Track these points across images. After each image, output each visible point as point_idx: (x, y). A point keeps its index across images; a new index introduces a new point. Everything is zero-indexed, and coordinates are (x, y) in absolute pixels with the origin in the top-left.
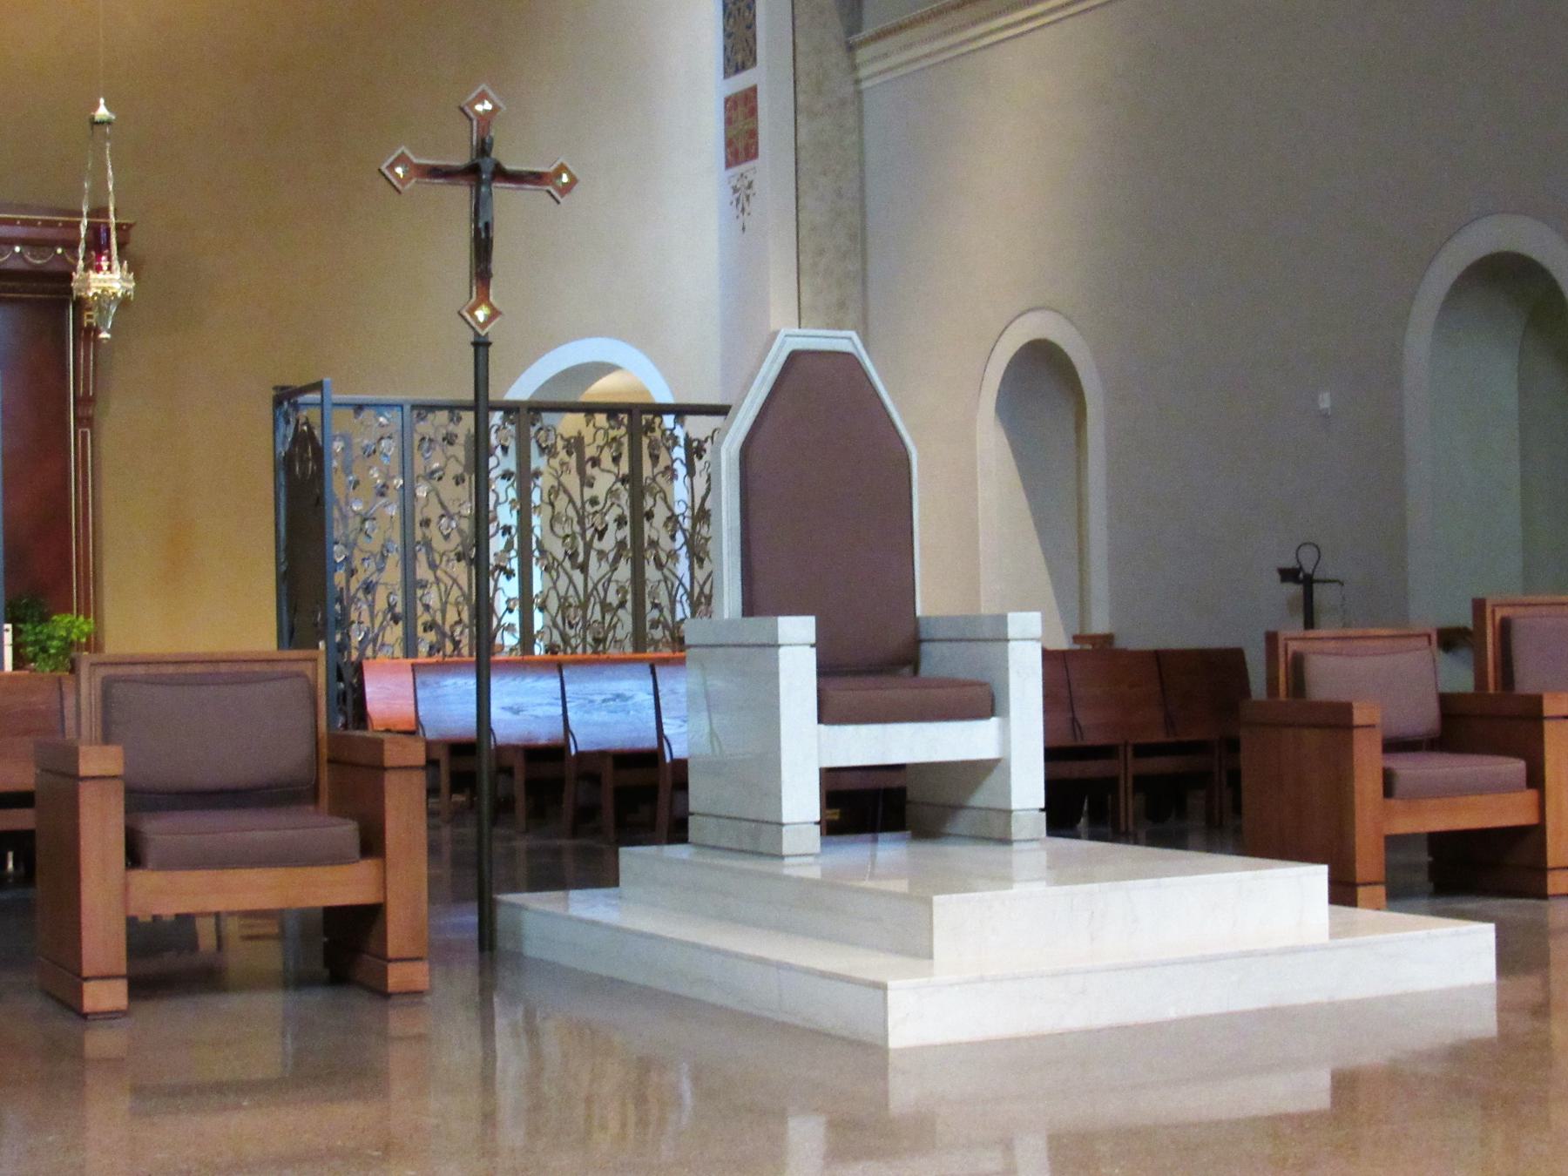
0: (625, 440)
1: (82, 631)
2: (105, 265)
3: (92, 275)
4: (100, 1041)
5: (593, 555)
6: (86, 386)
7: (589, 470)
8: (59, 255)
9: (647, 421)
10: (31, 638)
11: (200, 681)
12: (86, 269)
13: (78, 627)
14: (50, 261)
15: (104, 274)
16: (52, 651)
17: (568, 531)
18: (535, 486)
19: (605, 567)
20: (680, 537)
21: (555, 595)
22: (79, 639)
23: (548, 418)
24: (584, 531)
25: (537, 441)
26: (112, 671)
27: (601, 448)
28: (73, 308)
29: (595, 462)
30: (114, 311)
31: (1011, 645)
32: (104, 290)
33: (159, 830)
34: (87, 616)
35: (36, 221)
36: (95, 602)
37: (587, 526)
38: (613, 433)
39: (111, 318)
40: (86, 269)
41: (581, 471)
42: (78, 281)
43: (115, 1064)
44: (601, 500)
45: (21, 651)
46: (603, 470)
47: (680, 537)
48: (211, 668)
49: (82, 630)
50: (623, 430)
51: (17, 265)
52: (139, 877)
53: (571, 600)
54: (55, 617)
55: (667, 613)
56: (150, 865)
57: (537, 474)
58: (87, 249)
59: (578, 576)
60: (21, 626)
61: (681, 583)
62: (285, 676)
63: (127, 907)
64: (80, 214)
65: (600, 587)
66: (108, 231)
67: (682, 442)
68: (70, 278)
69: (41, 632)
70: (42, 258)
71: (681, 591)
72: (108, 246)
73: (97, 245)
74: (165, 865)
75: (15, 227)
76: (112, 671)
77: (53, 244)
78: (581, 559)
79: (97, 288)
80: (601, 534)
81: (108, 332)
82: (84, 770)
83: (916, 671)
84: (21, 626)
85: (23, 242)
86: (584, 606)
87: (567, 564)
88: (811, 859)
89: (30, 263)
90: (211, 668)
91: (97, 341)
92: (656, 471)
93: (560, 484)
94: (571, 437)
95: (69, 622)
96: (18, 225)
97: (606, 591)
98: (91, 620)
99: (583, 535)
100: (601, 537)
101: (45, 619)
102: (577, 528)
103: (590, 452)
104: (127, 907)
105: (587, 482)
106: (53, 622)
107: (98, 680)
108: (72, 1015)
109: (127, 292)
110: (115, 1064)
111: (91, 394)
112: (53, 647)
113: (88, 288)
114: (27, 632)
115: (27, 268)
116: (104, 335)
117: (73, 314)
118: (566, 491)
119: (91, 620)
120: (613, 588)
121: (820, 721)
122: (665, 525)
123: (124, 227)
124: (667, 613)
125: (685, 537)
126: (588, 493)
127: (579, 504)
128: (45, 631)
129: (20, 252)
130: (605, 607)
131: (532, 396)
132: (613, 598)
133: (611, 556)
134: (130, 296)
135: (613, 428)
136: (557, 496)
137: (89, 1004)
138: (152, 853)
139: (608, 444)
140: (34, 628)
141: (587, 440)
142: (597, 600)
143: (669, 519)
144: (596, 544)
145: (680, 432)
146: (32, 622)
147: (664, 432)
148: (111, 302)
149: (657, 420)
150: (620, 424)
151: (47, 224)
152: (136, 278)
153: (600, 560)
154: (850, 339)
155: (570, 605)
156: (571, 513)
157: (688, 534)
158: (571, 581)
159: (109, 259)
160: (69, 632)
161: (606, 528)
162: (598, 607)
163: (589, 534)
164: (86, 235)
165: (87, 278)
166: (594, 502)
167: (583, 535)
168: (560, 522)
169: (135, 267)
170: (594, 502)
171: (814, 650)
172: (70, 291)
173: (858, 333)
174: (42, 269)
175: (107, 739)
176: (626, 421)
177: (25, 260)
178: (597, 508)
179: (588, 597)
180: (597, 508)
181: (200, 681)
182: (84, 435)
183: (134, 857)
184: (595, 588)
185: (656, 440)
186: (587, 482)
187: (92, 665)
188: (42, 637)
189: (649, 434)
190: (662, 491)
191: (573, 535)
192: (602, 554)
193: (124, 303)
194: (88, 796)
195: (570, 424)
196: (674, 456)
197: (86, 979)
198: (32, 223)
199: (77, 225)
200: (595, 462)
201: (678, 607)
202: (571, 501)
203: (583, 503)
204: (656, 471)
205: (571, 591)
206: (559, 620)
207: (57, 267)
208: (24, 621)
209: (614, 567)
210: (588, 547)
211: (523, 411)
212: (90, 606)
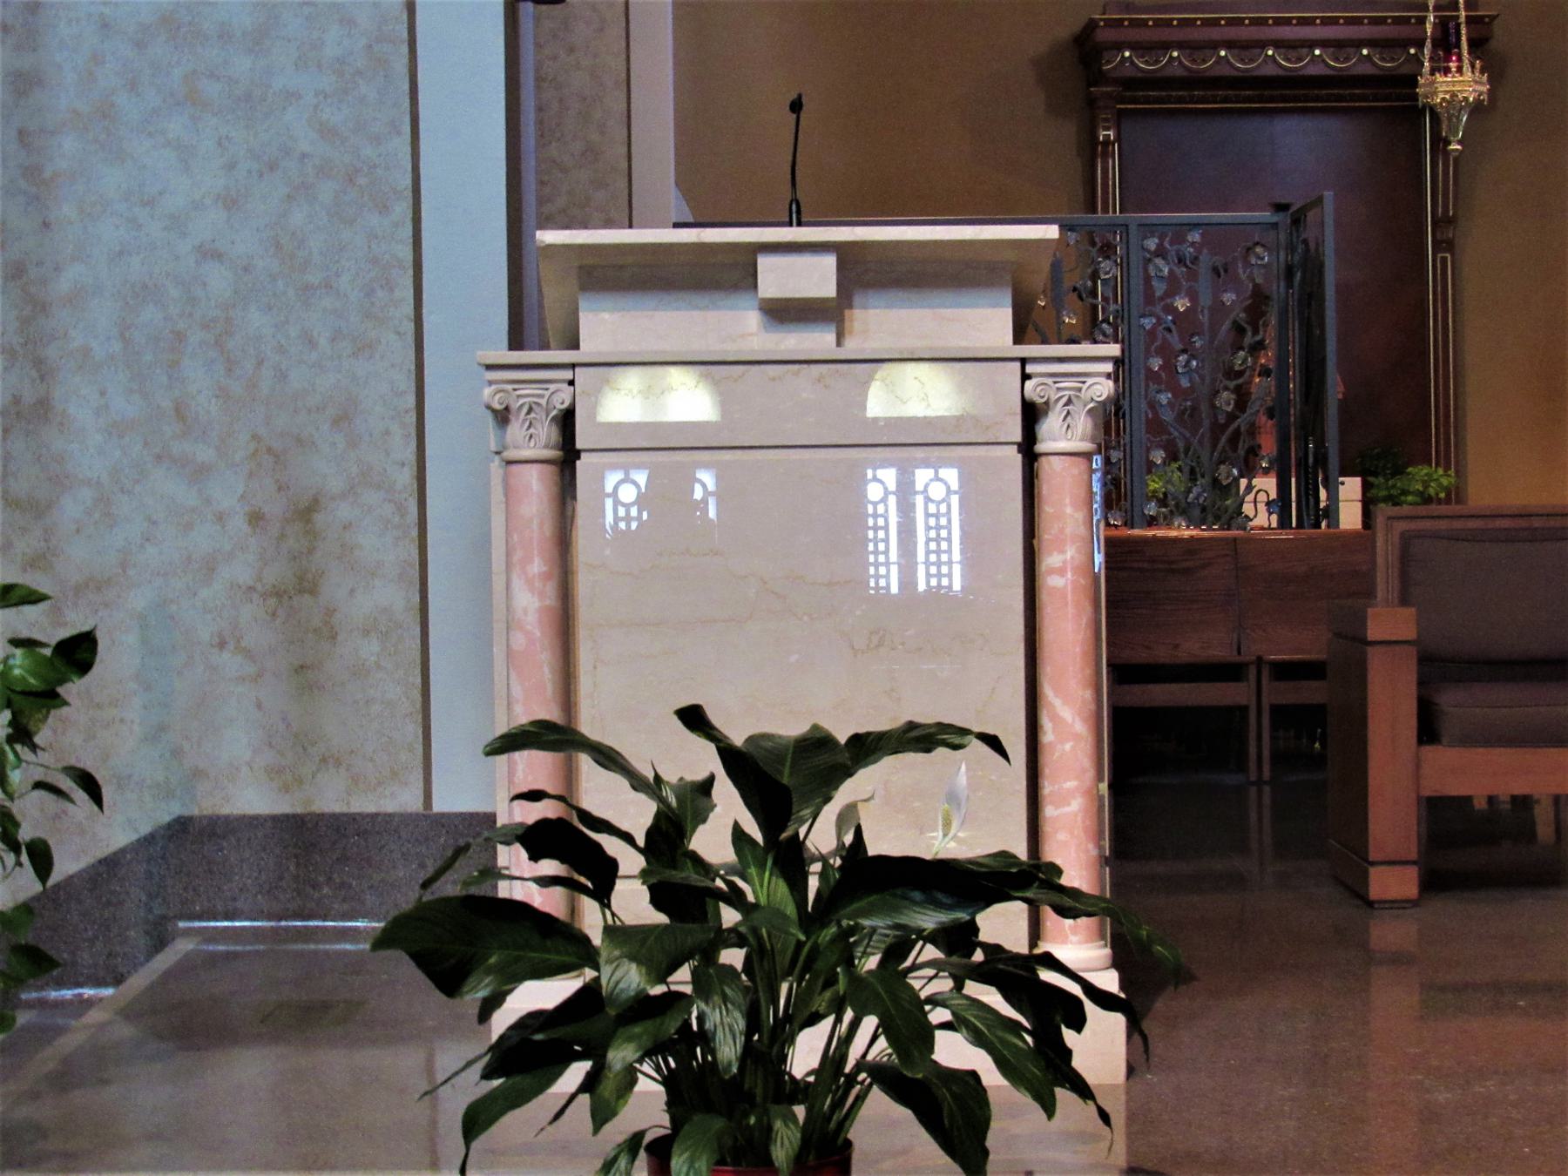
1: (1440, 485)
2: (1453, 65)
3: (1439, 78)
4: (1389, 933)
8: (1318, 56)
10: (1383, 493)
11: (1509, 537)
12: (1432, 72)
13: (1436, 480)
14: (1258, 67)
15: (1454, 77)
22: (1437, 494)
26: (1413, 525)
30: (1465, 119)
32: (1454, 95)
33: (1451, 700)
34: (1447, 468)
35: (1386, 18)
39: (1461, 128)
40: (1432, 72)
42: (1424, 85)
43: (1398, 960)
48: (1523, 523)
49: (1441, 483)
51: (1270, 70)
52: (1429, 752)
54: (1410, 469)
56: (1445, 740)
58: (1435, 45)
60: (1371, 479)
64: (1427, 10)
66: (1458, 25)
68: (1415, 84)
69: (1394, 486)
70: (1393, 60)
72: (1458, 45)
73: (1445, 43)
74: (1468, 740)
75: (1361, 28)
76: (1413, 525)
77: (1404, 44)
79: (1446, 92)
81: (1459, 142)
82: (1372, 634)
84: (1371, 479)
85: (1323, 44)
90: (1523, 523)
91: (1446, 153)
95: (1426, 475)
96: (1389, 24)
98: (1452, 472)
101: (1399, 471)
106: (1409, 474)
108: (1360, 902)
109: (1479, 96)
110: (1398, 960)
111: (1451, 214)
113: (1435, 93)
114: (1378, 486)
116: (1455, 146)
117: (1430, 122)
119: (1452, 472)
123: (1487, 20)
128: (1399, 485)
129: (1368, 55)
134: (1484, 100)
137: (1375, 892)
140: (1387, 480)
146: (1385, 475)
148: (1461, 108)
151: (1398, 21)
152: (1490, 81)
159: (1460, 59)
160: (1426, 485)
164: (1432, 33)
165: (1434, 82)
169: (1495, 69)
172: (1415, 97)
174: (1394, 73)
175: (1404, 601)
177: (1374, 64)
181: (1535, 536)
182: (1444, 260)
183: (1428, 731)
187: (1389, 518)
188: (1394, 492)
193: (1477, 109)
194: (1377, 664)
197: (1373, 864)
198: (1333, 21)
199: (1422, 21)
207: (1405, 70)
208: (1375, 474)
212: (1451, 456)
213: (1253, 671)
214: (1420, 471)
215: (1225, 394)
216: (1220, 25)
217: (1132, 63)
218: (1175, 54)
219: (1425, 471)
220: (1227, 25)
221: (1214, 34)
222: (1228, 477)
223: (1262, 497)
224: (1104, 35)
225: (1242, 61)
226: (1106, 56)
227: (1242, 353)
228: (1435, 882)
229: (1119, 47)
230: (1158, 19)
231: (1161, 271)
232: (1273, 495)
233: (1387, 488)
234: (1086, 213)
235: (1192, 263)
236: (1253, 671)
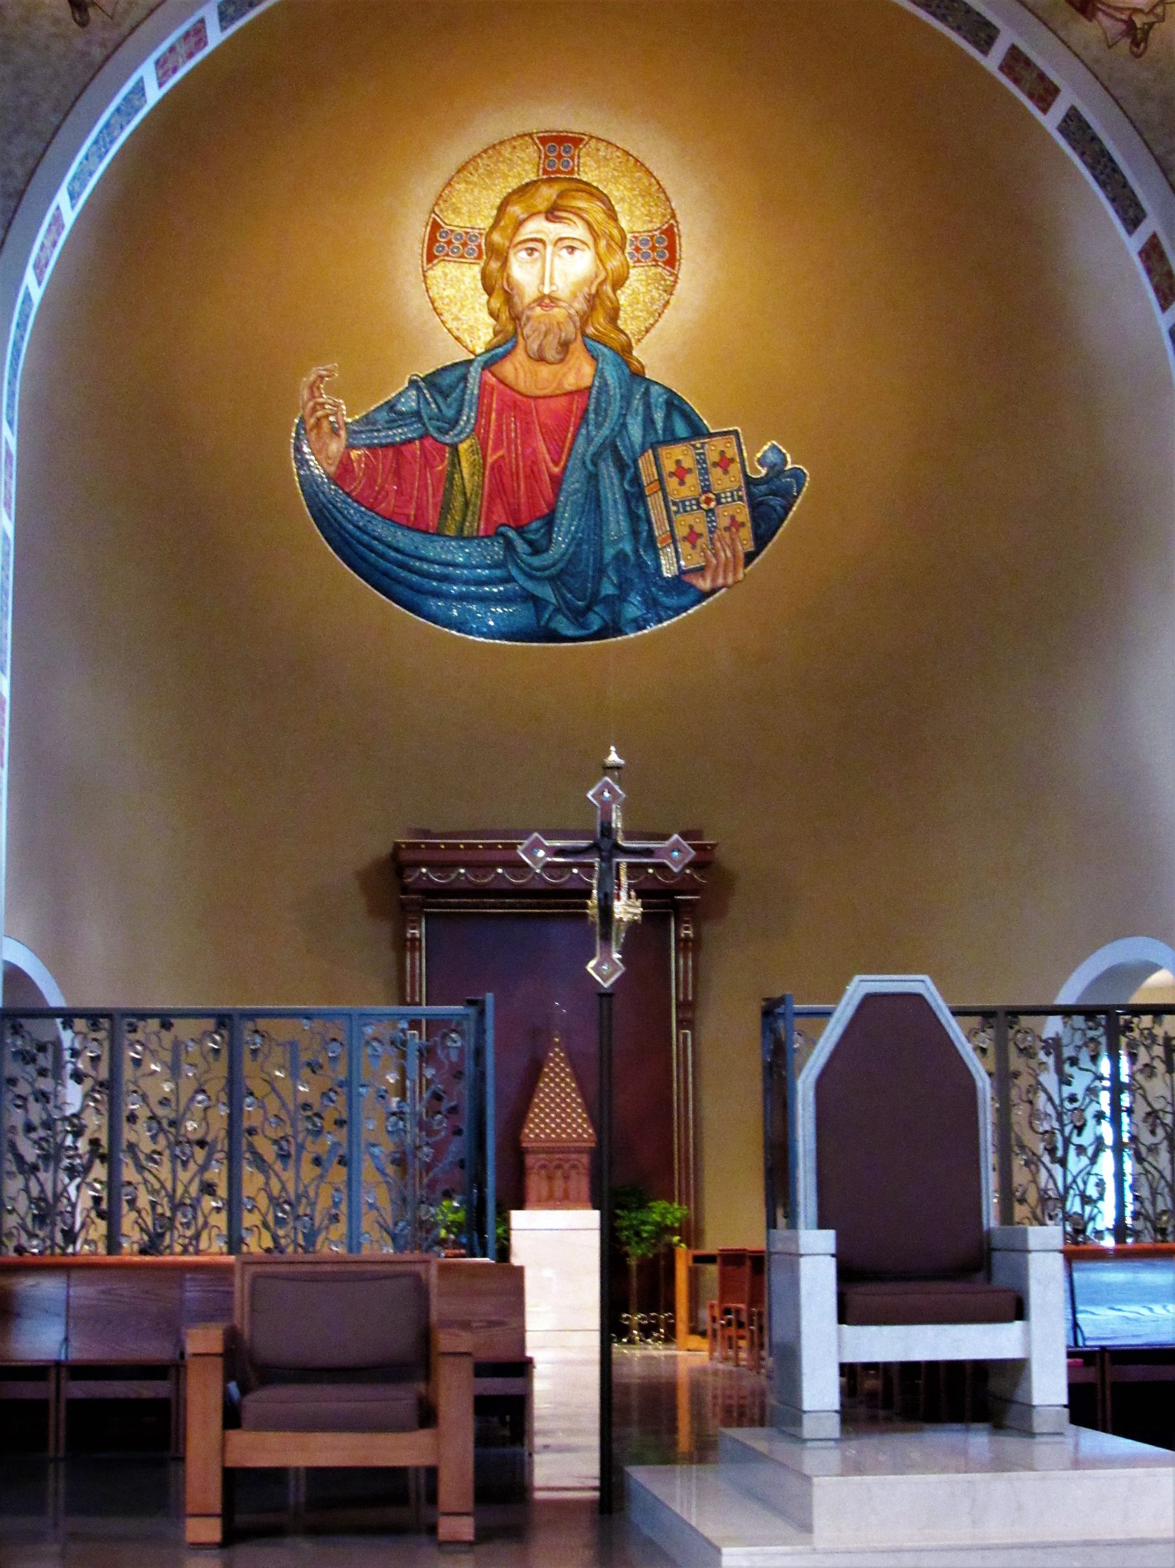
0: (1103, 1040)
5: (1072, 1151)
6: (686, 995)
7: (1067, 1068)
9: (1126, 1021)
16: (645, 1235)
17: (1047, 1128)
18: (1014, 1085)
19: (1085, 1161)
20: (1160, 1132)
21: (1035, 1190)
22: (672, 1224)
23: (1025, 1021)
24: (1062, 1125)
25: (1015, 1044)
27: (1079, 1048)
28: (675, 923)
29: (1074, 1061)
31: (1031, 1256)
36: (696, 1192)
37: (1066, 1122)
38: (1091, 1034)
41: (1059, 1071)
44: (1080, 1097)
45: (617, 1234)
46: (1081, 1069)
47: (1160, 1132)
50: (1101, 1030)
52: (235, 1436)
53: (1050, 1193)
54: (652, 1204)
55: (1148, 1205)
57: (1016, 1075)
59: (1057, 1170)
61: (1162, 1177)
62: (397, 1276)
63: (223, 1460)
65: (1079, 1181)
67: (1161, 1041)
71: (1163, 1183)
78: (1060, 1153)
80: (1080, 1129)
83: (989, 1278)
86: (1063, 1199)
87: (1046, 1159)
88: (831, 1444)
89: (663, 884)
92: (1135, 1068)
93: (1039, 1083)
94: (1050, 1039)
97: (1085, 1183)
99: (1062, 1131)
100: (1079, 1134)
101: (642, 1205)
102: (1056, 1125)
103: (1068, 1052)
104: (223, 1460)
105: (1065, 1080)
107: (247, 1278)
112: (646, 1232)
115: (658, 887)
118: (1045, 1091)
120: (1093, 1180)
121: (842, 1318)
122: (1145, 1121)
124: (1148, 1205)
125: (1166, 1131)
126: (1067, 1091)
127: (1057, 1102)
130: (1086, 1200)
131: (1079, 998)
132: (1092, 1192)
133: (1090, 1151)
135: (1090, 1029)
136: (1035, 1093)
138: (248, 1415)
139: (1086, 1045)
141: (1065, 1041)
142: (1077, 1192)
143: (1149, 1114)
144: (1076, 1140)
145: (1159, 1031)
147: (1141, 1030)
149: (1135, 1020)
150: (1099, 1025)
153: (1078, 1155)
154: (923, 981)
155: (1050, 1198)
156: (1050, 1110)
157: (1169, 1130)
158: (1051, 1176)
160: (663, 1216)
161: (1084, 1125)
162: (1077, 1200)
163: (1067, 1130)
166: (1073, 1099)
167: (1062, 1131)
168: (1039, 1119)
170: (1073, 1099)
171: (833, 1261)
172: (643, 906)
173: (931, 977)
176: (1103, 1022)
178: (1076, 1105)
179: (1067, 1188)
180: (1076, 1105)
182: (685, 1035)
183: (232, 1418)
184: (1074, 1181)
185: (1135, 1039)
186: (1065, 1080)
189: (1128, 1034)
190: (1141, 1088)
191: (1051, 1133)
192: (1081, 1149)
195: (1053, 1026)
196: (1154, 1054)
200: (1074, 1061)
201: (1159, 1199)
202: (1050, 1099)
203: (1062, 1101)
204: (1135, 1068)
205: (1051, 1185)
206: (1039, 1211)
209: (1093, 1160)
210: (1067, 1142)
211: (1001, 1015)
212: (693, 1195)
213: (53, 1375)
214: (660, 1205)
215: (426, 1149)
216: (460, 849)
217: (428, 877)
218: (462, 871)
219: (663, 1206)
220: (446, 848)
221: (451, 856)
222: (426, 1214)
223: (215, 1231)
224: (406, 856)
225: (515, 877)
226: (408, 872)
227: (439, 1117)
228: (232, 1537)
229: (418, 864)
230: (469, 844)
231: (376, 1051)
232: (225, 1232)
233: (630, 1219)
234: (388, 1005)
235: (402, 1045)
236: (53, 1375)
